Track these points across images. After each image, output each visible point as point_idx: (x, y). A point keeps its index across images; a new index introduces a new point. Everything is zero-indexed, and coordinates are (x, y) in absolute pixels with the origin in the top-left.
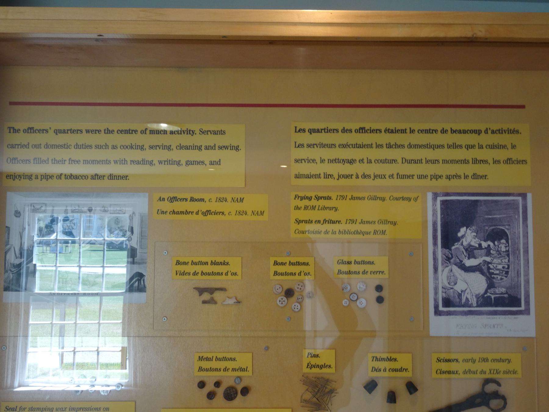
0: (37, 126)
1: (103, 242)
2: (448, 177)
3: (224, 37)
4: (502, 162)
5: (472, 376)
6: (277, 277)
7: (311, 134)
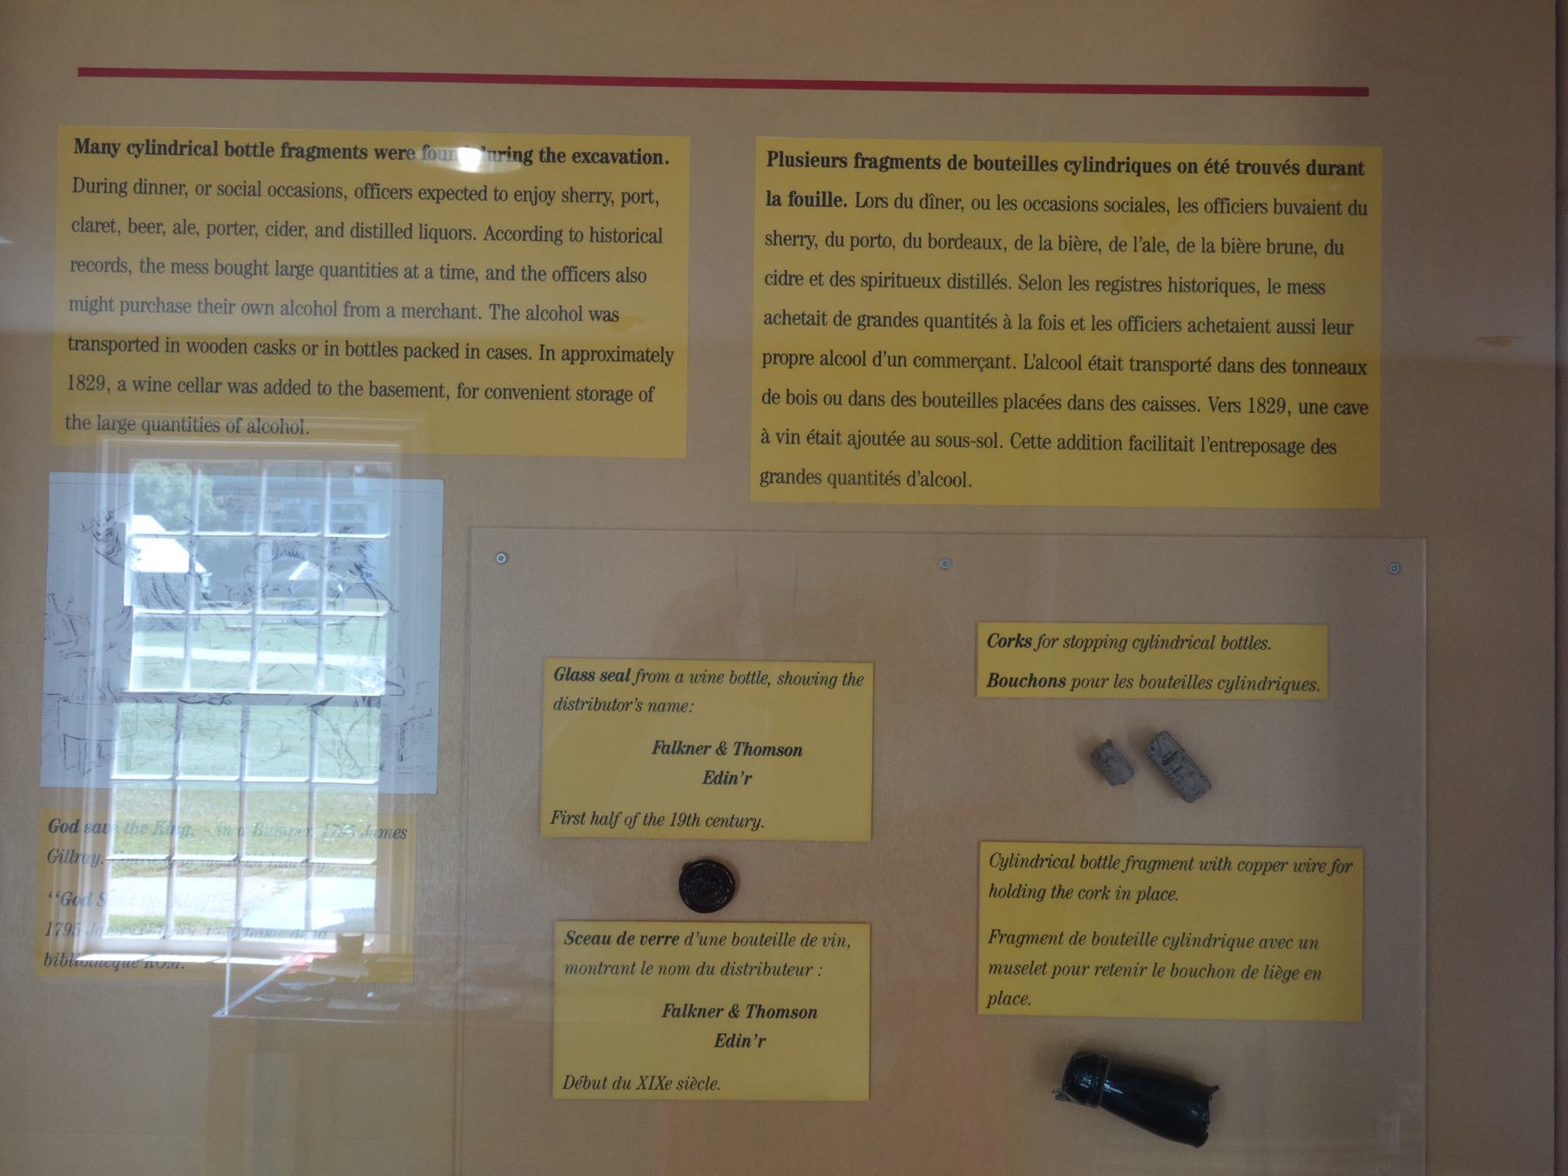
1: (252, 541)
2: (868, 282)
5: (591, 1094)
6: (998, 691)
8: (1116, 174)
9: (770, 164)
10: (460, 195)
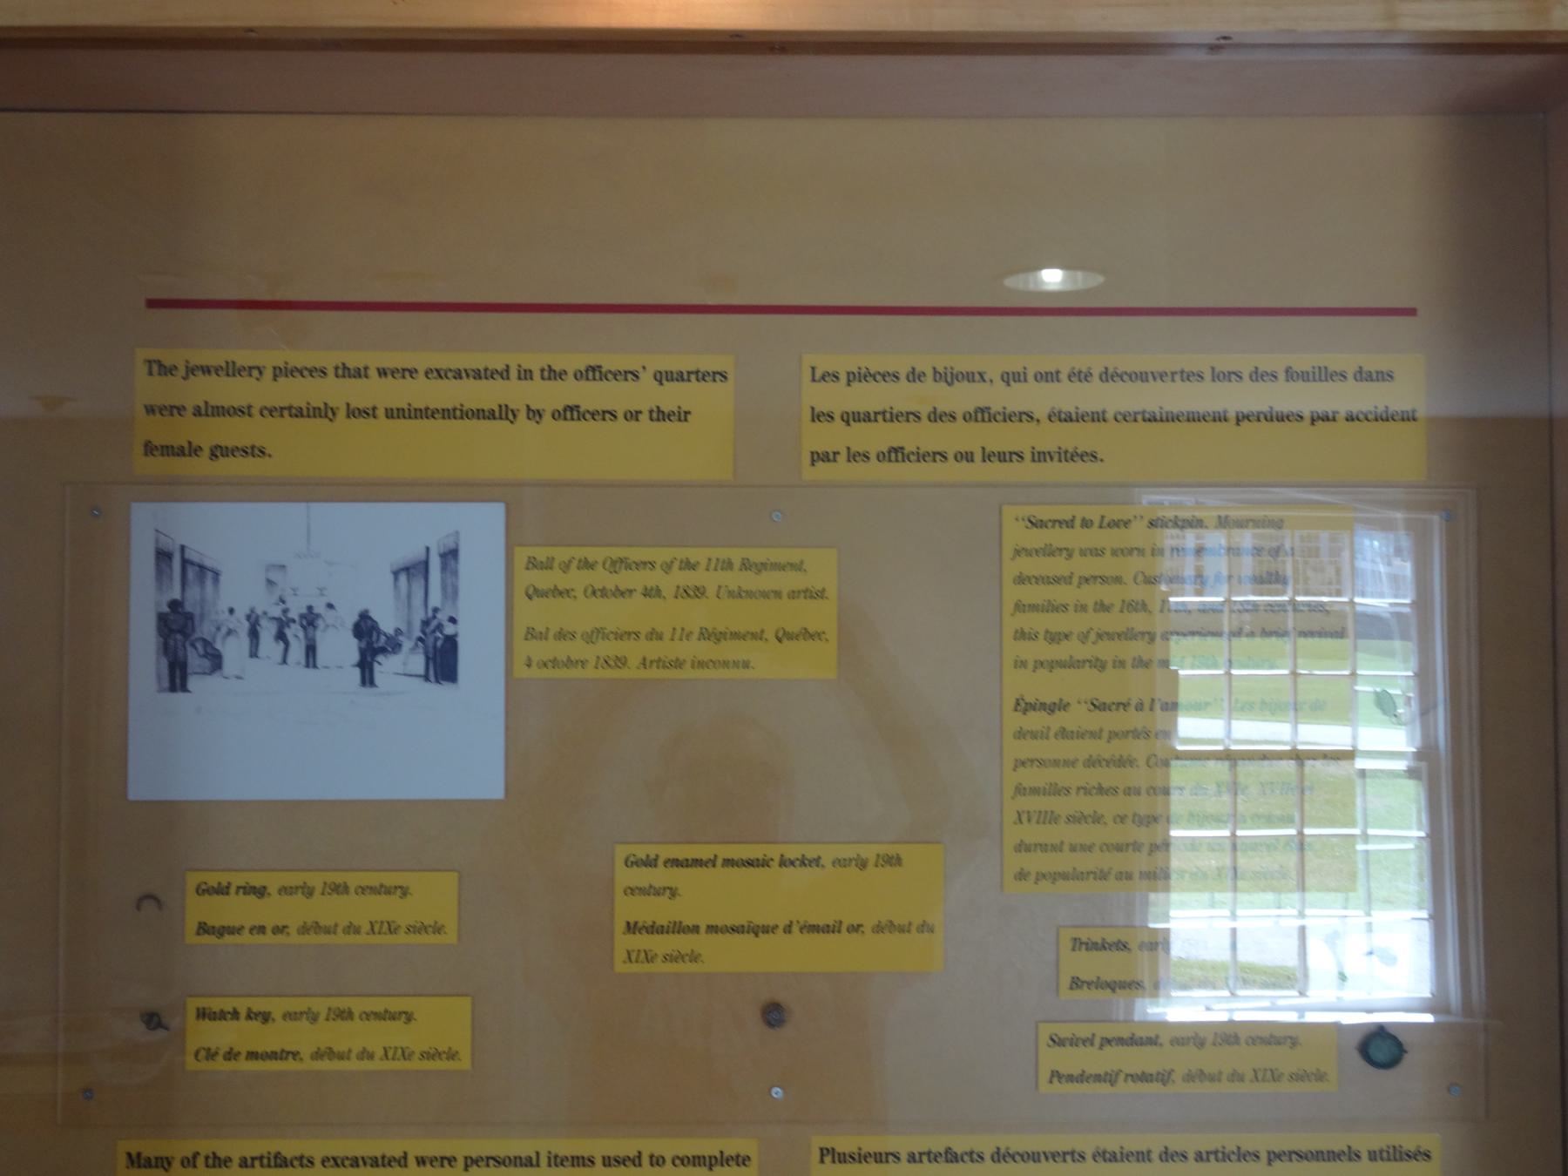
0: (609, 362)
3: (251, 30)
7: (661, 383)
9: (822, 1161)
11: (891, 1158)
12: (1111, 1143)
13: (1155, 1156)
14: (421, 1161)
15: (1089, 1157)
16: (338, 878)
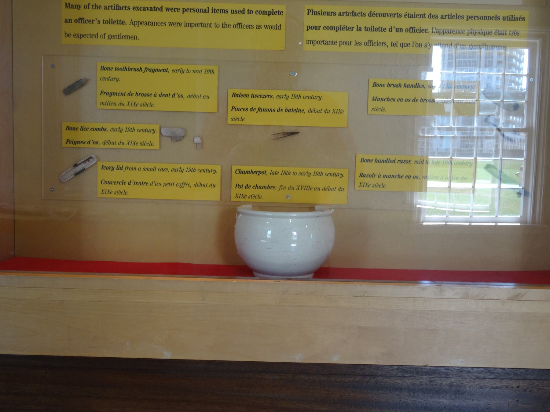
4: (363, 43)
8: (330, 16)
9: (308, 14)
10: (88, 36)
11: (333, 14)
12: (411, 11)
13: (426, 16)
14: (167, 9)
15: (403, 15)
16: (131, 126)
